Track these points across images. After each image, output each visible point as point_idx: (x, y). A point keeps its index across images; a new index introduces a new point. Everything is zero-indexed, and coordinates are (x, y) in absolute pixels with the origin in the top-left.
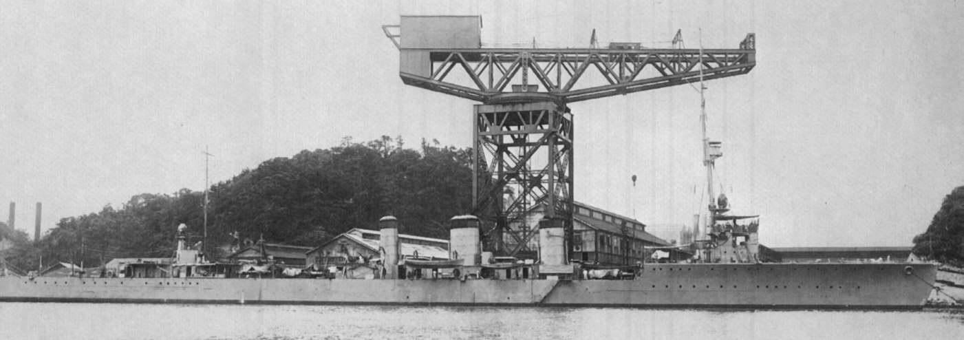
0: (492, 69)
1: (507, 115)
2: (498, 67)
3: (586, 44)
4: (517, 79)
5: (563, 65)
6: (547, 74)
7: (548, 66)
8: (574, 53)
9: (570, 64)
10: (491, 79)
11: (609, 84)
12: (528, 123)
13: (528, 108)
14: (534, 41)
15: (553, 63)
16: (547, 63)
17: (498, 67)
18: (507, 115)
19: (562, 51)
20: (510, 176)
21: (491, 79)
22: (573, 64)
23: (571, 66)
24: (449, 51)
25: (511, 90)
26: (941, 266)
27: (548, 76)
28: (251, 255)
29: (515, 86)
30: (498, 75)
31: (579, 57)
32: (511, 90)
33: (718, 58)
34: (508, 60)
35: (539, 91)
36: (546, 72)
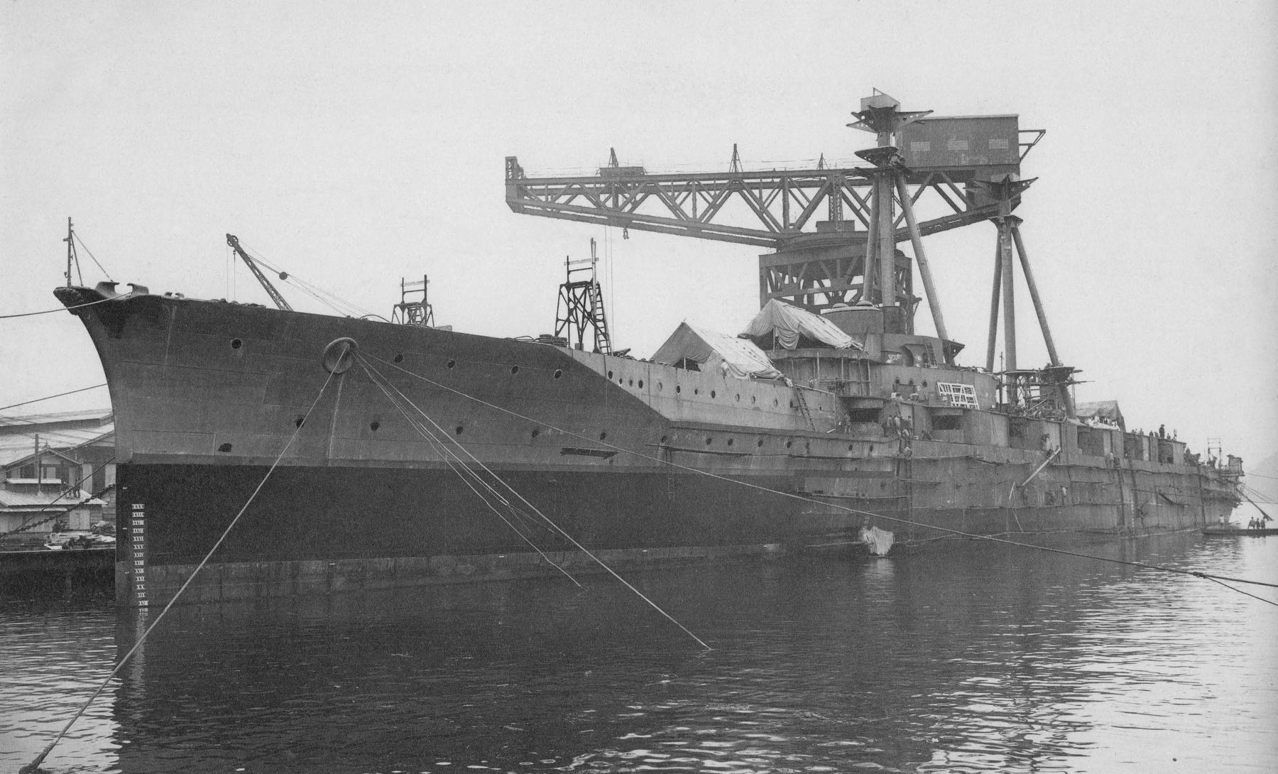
0: (694, 200)
1: (805, 267)
2: (703, 197)
3: (726, 168)
4: (822, 213)
5: (791, 192)
6: (768, 205)
7: (772, 192)
8: (710, 180)
9: (709, 194)
10: (695, 209)
11: (954, 213)
12: (835, 277)
13: (834, 255)
14: (822, 158)
15: (777, 190)
16: (772, 190)
17: (703, 197)
18: (805, 267)
19: (790, 174)
20: (1021, 385)
21: (695, 209)
22: (756, 192)
23: (678, 196)
24: (928, 170)
25: (814, 230)
26: (1058, 649)
27: (768, 209)
28: (781, 683)
29: (820, 222)
30: (702, 206)
31: (764, 183)
32: (814, 230)
33: (704, 185)
34: (809, 185)
35: (857, 229)
36: (766, 205)
